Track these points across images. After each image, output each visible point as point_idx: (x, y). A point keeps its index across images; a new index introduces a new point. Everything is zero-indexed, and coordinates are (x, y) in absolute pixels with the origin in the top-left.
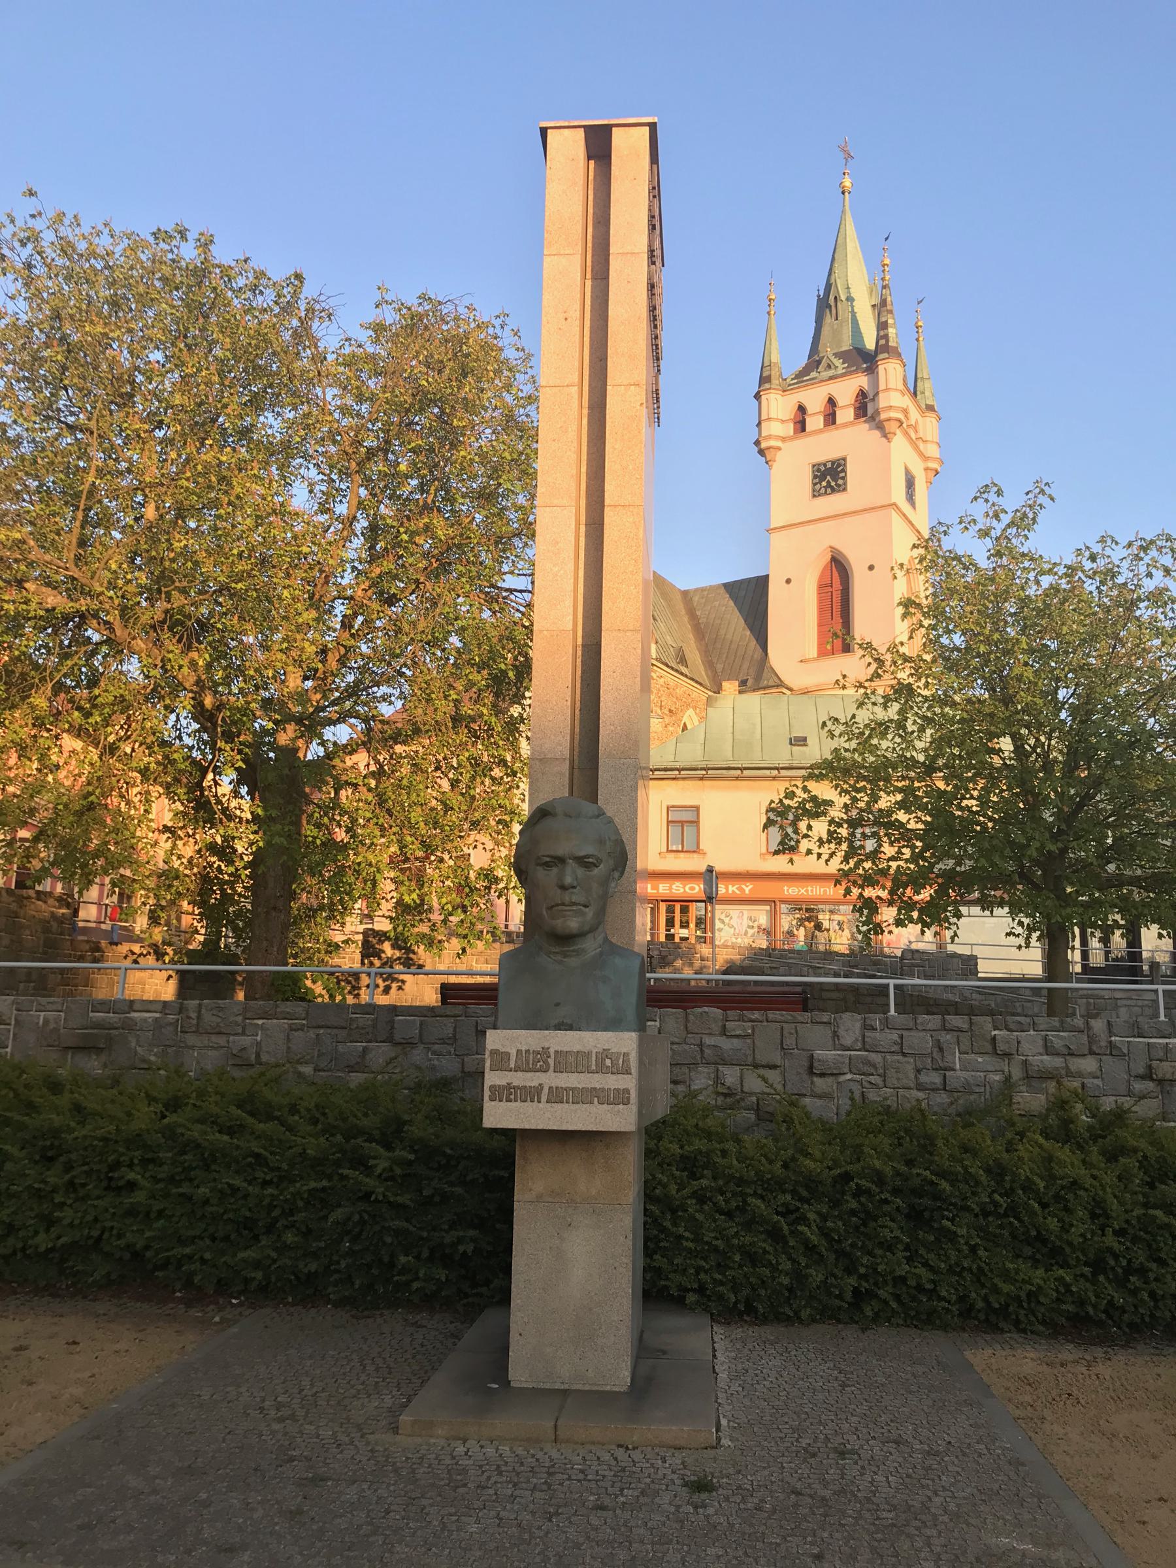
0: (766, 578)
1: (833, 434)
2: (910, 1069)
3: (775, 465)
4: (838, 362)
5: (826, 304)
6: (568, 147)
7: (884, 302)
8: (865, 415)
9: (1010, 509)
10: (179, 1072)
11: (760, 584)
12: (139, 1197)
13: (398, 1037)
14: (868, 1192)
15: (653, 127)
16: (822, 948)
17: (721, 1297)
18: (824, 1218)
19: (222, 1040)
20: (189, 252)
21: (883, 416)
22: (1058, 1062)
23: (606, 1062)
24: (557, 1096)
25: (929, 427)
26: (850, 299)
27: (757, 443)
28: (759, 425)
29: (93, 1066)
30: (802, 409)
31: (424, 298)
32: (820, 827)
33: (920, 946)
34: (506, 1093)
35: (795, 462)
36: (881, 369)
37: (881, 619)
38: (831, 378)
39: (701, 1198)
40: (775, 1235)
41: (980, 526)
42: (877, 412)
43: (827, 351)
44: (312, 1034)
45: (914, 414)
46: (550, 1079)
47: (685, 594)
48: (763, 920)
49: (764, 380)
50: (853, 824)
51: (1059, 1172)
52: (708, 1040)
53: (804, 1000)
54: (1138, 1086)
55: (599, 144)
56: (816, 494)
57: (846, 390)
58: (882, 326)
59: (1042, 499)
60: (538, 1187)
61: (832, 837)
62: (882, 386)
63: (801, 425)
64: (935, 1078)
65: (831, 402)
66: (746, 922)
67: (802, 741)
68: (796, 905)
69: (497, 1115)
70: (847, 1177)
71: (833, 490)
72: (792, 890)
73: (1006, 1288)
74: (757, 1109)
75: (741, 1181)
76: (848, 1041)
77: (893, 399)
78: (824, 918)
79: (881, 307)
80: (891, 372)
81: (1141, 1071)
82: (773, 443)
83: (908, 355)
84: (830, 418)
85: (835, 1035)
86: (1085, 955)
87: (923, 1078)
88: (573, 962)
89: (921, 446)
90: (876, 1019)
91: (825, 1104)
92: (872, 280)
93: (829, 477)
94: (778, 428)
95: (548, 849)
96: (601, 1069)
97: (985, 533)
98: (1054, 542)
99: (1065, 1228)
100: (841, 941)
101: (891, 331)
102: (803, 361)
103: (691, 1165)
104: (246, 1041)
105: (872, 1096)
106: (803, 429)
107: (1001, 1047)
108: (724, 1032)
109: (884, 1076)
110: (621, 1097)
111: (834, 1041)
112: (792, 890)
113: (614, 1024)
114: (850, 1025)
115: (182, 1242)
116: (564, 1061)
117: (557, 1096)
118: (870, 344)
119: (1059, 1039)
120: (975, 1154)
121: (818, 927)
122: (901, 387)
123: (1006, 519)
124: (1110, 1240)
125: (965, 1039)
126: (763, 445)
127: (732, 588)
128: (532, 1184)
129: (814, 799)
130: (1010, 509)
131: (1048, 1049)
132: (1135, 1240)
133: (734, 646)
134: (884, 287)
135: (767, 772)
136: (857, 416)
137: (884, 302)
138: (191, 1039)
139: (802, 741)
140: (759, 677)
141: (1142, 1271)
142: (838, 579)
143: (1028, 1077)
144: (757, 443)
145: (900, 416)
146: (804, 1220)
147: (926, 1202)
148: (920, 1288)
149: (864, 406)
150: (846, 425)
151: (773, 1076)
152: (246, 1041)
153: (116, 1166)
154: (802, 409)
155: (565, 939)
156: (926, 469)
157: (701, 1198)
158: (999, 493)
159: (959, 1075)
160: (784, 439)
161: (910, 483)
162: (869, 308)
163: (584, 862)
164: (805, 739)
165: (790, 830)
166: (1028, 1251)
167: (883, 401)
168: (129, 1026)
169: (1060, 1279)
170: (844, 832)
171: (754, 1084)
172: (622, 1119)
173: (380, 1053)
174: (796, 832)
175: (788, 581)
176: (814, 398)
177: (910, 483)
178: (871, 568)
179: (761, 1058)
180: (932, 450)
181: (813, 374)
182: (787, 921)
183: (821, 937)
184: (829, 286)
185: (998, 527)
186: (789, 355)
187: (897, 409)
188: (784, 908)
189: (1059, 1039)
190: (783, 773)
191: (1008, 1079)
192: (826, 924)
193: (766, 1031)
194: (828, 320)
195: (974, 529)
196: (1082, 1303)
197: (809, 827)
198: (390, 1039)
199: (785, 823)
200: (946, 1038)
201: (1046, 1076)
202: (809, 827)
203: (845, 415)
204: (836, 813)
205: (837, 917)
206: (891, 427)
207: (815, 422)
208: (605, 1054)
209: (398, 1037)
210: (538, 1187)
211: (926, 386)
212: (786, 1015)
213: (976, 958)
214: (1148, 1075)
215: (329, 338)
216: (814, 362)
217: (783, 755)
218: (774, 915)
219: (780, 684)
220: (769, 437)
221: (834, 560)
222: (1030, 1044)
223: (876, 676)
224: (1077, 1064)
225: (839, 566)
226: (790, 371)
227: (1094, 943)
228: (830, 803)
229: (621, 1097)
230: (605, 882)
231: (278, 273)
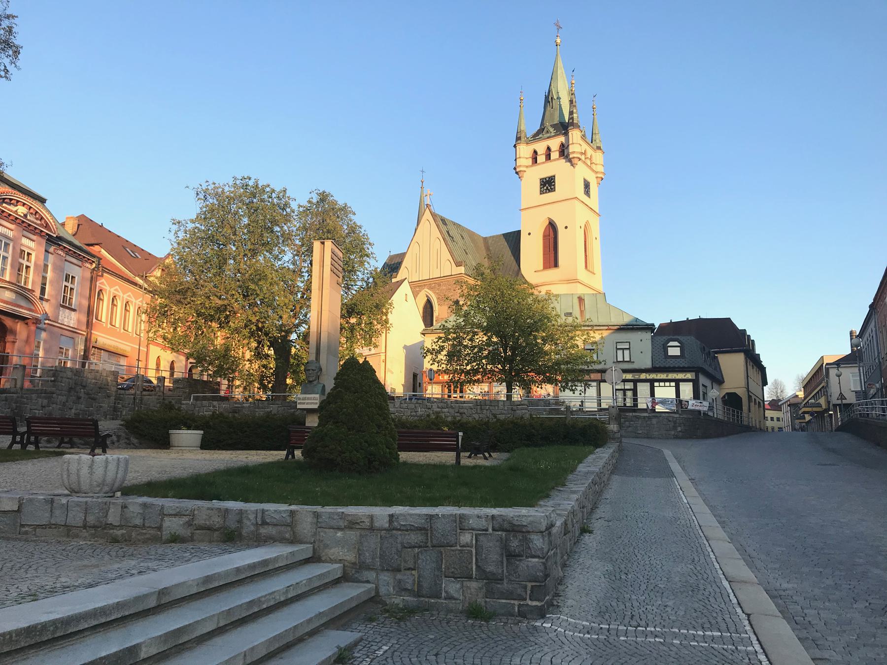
0: (519, 232)
1: (549, 164)
4: (552, 130)
5: (548, 100)
11: (518, 233)
21: (571, 156)
23: (314, 399)
25: (598, 157)
26: (559, 98)
27: (515, 169)
30: (535, 152)
34: (300, 403)
35: (533, 176)
45: (590, 152)
47: (485, 239)
49: (518, 139)
56: (542, 193)
57: (555, 143)
58: (571, 113)
63: (535, 160)
65: (549, 149)
82: (521, 169)
84: (548, 157)
89: (594, 167)
93: (548, 184)
94: (524, 162)
116: (308, 399)
126: (518, 170)
127: (507, 236)
136: (560, 156)
142: (552, 232)
149: (564, 151)
150: (555, 160)
154: (535, 152)
159: (419, 413)
160: (527, 167)
161: (587, 185)
168: (243, 407)
175: (529, 234)
176: (541, 147)
177: (587, 185)
178: (566, 227)
180: (600, 169)
186: (531, 126)
194: (549, 108)
203: (555, 155)
206: (575, 161)
207: (541, 158)
211: (597, 137)
215: (294, 205)
221: (550, 223)
225: (552, 227)
226: (530, 134)
231: (277, 190)
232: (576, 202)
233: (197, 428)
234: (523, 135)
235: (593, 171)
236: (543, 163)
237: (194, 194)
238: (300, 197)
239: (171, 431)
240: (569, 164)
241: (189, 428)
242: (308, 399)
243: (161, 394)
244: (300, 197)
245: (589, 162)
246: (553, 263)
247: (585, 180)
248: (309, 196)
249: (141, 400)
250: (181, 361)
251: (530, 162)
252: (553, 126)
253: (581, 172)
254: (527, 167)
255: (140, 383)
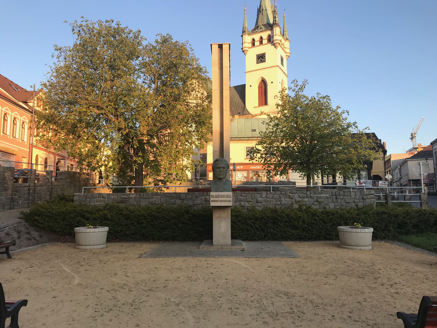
1: (262, 47)
2: (275, 201)
3: (247, 55)
4: (263, 27)
5: (260, 11)
6: (215, 48)
7: (275, 11)
8: (270, 42)
9: (299, 85)
10: (140, 206)
11: (244, 86)
12: (144, 225)
13: (181, 198)
14: (266, 219)
15: (230, 44)
16: (260, 181)
17: (243, 237)
18: (259, 223)
19: (148, 200)
20: (114, 25)
21: (275, 42)
22: (301, 199)
23: (228, 196)
24: (221, 201)
25: (287, 44)
26: (266, 10)
27: (242, 49)
28: (242, 44)
29: (122, 205)
30: (254, 40)
31: (168, 34)
32: (259, 155)
33: (283, 180)
34: (213, 201)
36: (274, 29)
37: (274, 98)
38: (261, 31)
39: (239, 221)
40: (251, 226)
41: (293, 89)
42: (273, 41)
43: (260, 24)
44: (165, 198)
45: (283, 41)
46: (220, 199)
48: (245, 175)
49: (244, 32)
50: (266, 154)
51: (297, 215)
52: (238, 197)
53: (255, 190)
54: (315, 203)
55: (221, 47)
57: (265, 35)
58: (274, 18)
59: (306, 83)
60: (216, 216)
61: (262, 157)
62: (275, 34)
63: (253, 44)
64: (279, 203)
65: (261, 38)
66: (241, 175)
67: (254, 130)
68: (253, 171)
69: (212, 204)
70: (263, 217)
71: (262, 62)
72: (252, 167)
73: (289, 233)
74: (247, 209)
75: (246, 218)
76: (264, 197)
77: (277, 37)
78: (260, 174)
79: (274, 12)
80: (277, 30)
81: (316, 200)
83: (281, 25)
84: (261, 42)
85: (261, 196)
86: (322, 181)
87: (277, 203)
88: (222, 182)
89: (285, 49)
90: (269, 193)
91: (259, 208)
92: (272, 4)
93: (261, 58)
94: (247, 45)
95: (218, 166)
96: (227, 197)
97: (294, 91)
98: (310, 93)
99: (298, 224)
100: (265, 179)
101: (277, 19)
102: (254, 27)
103: (237, 216)
104: (153, 200)
105: (268, 206)
106: (254, 45)
107: (291, 197)
108: (241, 196)
109: (270, 203)
110: (230, 201)
111: (261, 197)
112: (252, 167)
113: (228, 191)
114: (264, 194)
115: (151, 232)
116: (222, 196)
117: (221, 201)
118: (271, 22)
119: (301, 195)
120: (284, 213)
121: (259, 176)
122: (279, 34)
123: (298, 87)
124: (305, 226)
125: (284, 196)
126: (244, 49)
128: (216, 216)
129: (257, 149)
130: (299, 85)
131: (299, 197)
132: (309, 225)
133: (237, 103)
134: (275, 7)
135: (246, 139)
136: (268, 42)
137: (275, 11)
138: (142, 200)
139: (254, 130)
140: (243, 112)
141: (310, 230)
143: (296, 202)
144: (242, 49)
145: (279, 42)
146: (256, 224)
147: (276, 221)
148: (275, 234)
149: (270, 39)
150: (265, 44)
151: (250, 203)
152: (153, 200)
153: (140, 220)
154: (254, 40)
155: (220, 179)
156: (286, 56)
157: (239, 221)
158: (297, 82)
159: (284, 202)
160: (249, 48)
161: (282, 60)
162: (271, 12)
163: (223, 168)
164: (255, 130)
165: (252, 156)
166: (292, 228)
167: (275, 38)
169: (297, 232)
170: (264, 156)
171: (247, 204)
172: (230, 204)
173: (178, 202)
174: (254, 156)
175: (251, 86)
176: (257, 37)
177: (282, 60)
178: (272, 83)
179: (248, 200)
181: (257, 30)
182: (251, 175)
183: (260, 178)
184: (260, 6)
185: (297, 89)
187: (278, 40)
188: (251, 172)
189: (301, 195)
190: (250, 139)
191: (292, 203)
192: (261, 175)
193: (249, 196)
194: (260, 15)
195: (291, 90)
196: (301, 236)
197: (256, 155)
198: (180, 199)
199: (251, 152)
200: (281, 195)
201: (299, 202)
202: (256, 155)
203: (265, 41)
204: (262, 152)
205: (263, 174)
206: (277, 45)
207: (257, 43)
208: (228, 195)
209: (181, 198)
210: (216, 216)
212: (252, 192)
213: (295, 182)
214: (317, 201)
216: (257, 27)
217: (250, 134)
218: (248, 174)
219: (249, 113)
220: (245, 47)
221: (262, 80)
222: (296, 196)
223: (271, 122)
224: (304, 200)
227: (325, 179)
228: (261, 150)
229: (230, 201)
230: (226, 170)
232: (277, 67)
233: (103, 225)
234: (246, 30)
235: (285, 52)
236: (258, 46)
237: (70, 28)
238: (150, 38)
239: (77, 229)
240: (273, 47)
241: (95, 225)
242: (222, 196)
243: (50, 184)
244: (150, 38)
245: (283, 47)
246: (264, 103)
247: (281, 57)
248: (155, 38)
249: (35, 191)
250: (51, 158)
251: (250, 45)
252: (264, 25)
253: (279, 51)
254: (249, 48)
255: (28, 175)
